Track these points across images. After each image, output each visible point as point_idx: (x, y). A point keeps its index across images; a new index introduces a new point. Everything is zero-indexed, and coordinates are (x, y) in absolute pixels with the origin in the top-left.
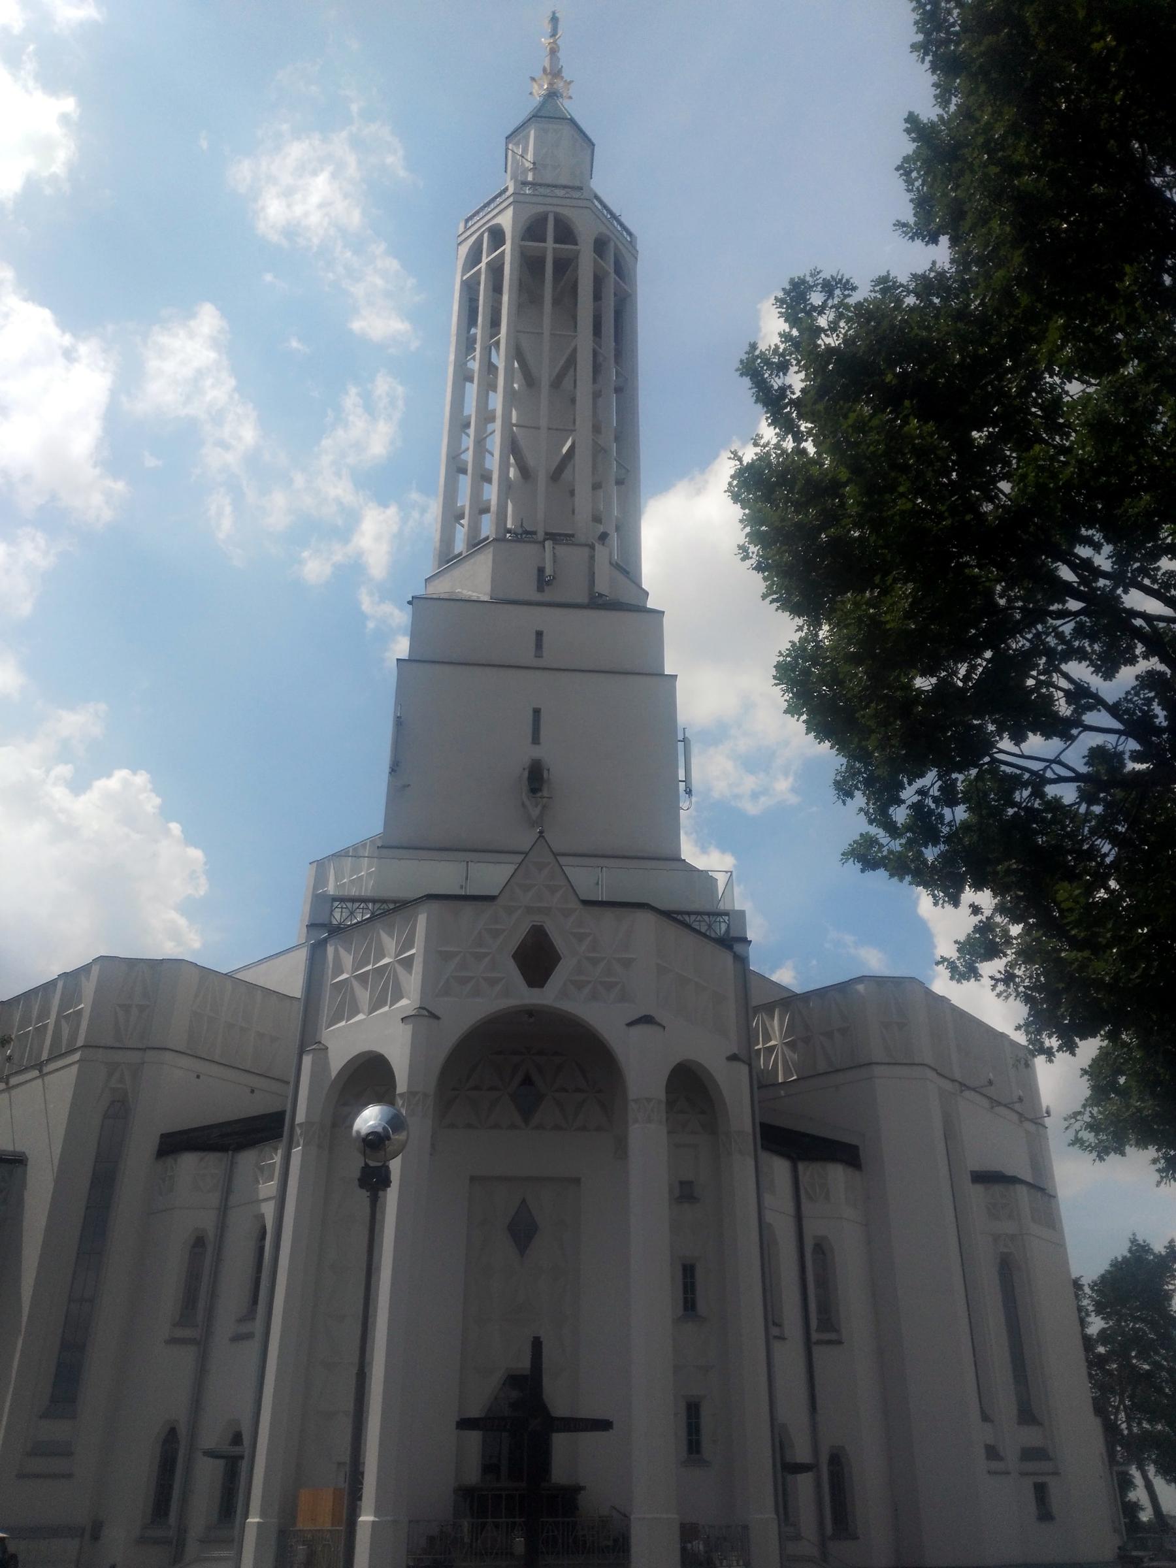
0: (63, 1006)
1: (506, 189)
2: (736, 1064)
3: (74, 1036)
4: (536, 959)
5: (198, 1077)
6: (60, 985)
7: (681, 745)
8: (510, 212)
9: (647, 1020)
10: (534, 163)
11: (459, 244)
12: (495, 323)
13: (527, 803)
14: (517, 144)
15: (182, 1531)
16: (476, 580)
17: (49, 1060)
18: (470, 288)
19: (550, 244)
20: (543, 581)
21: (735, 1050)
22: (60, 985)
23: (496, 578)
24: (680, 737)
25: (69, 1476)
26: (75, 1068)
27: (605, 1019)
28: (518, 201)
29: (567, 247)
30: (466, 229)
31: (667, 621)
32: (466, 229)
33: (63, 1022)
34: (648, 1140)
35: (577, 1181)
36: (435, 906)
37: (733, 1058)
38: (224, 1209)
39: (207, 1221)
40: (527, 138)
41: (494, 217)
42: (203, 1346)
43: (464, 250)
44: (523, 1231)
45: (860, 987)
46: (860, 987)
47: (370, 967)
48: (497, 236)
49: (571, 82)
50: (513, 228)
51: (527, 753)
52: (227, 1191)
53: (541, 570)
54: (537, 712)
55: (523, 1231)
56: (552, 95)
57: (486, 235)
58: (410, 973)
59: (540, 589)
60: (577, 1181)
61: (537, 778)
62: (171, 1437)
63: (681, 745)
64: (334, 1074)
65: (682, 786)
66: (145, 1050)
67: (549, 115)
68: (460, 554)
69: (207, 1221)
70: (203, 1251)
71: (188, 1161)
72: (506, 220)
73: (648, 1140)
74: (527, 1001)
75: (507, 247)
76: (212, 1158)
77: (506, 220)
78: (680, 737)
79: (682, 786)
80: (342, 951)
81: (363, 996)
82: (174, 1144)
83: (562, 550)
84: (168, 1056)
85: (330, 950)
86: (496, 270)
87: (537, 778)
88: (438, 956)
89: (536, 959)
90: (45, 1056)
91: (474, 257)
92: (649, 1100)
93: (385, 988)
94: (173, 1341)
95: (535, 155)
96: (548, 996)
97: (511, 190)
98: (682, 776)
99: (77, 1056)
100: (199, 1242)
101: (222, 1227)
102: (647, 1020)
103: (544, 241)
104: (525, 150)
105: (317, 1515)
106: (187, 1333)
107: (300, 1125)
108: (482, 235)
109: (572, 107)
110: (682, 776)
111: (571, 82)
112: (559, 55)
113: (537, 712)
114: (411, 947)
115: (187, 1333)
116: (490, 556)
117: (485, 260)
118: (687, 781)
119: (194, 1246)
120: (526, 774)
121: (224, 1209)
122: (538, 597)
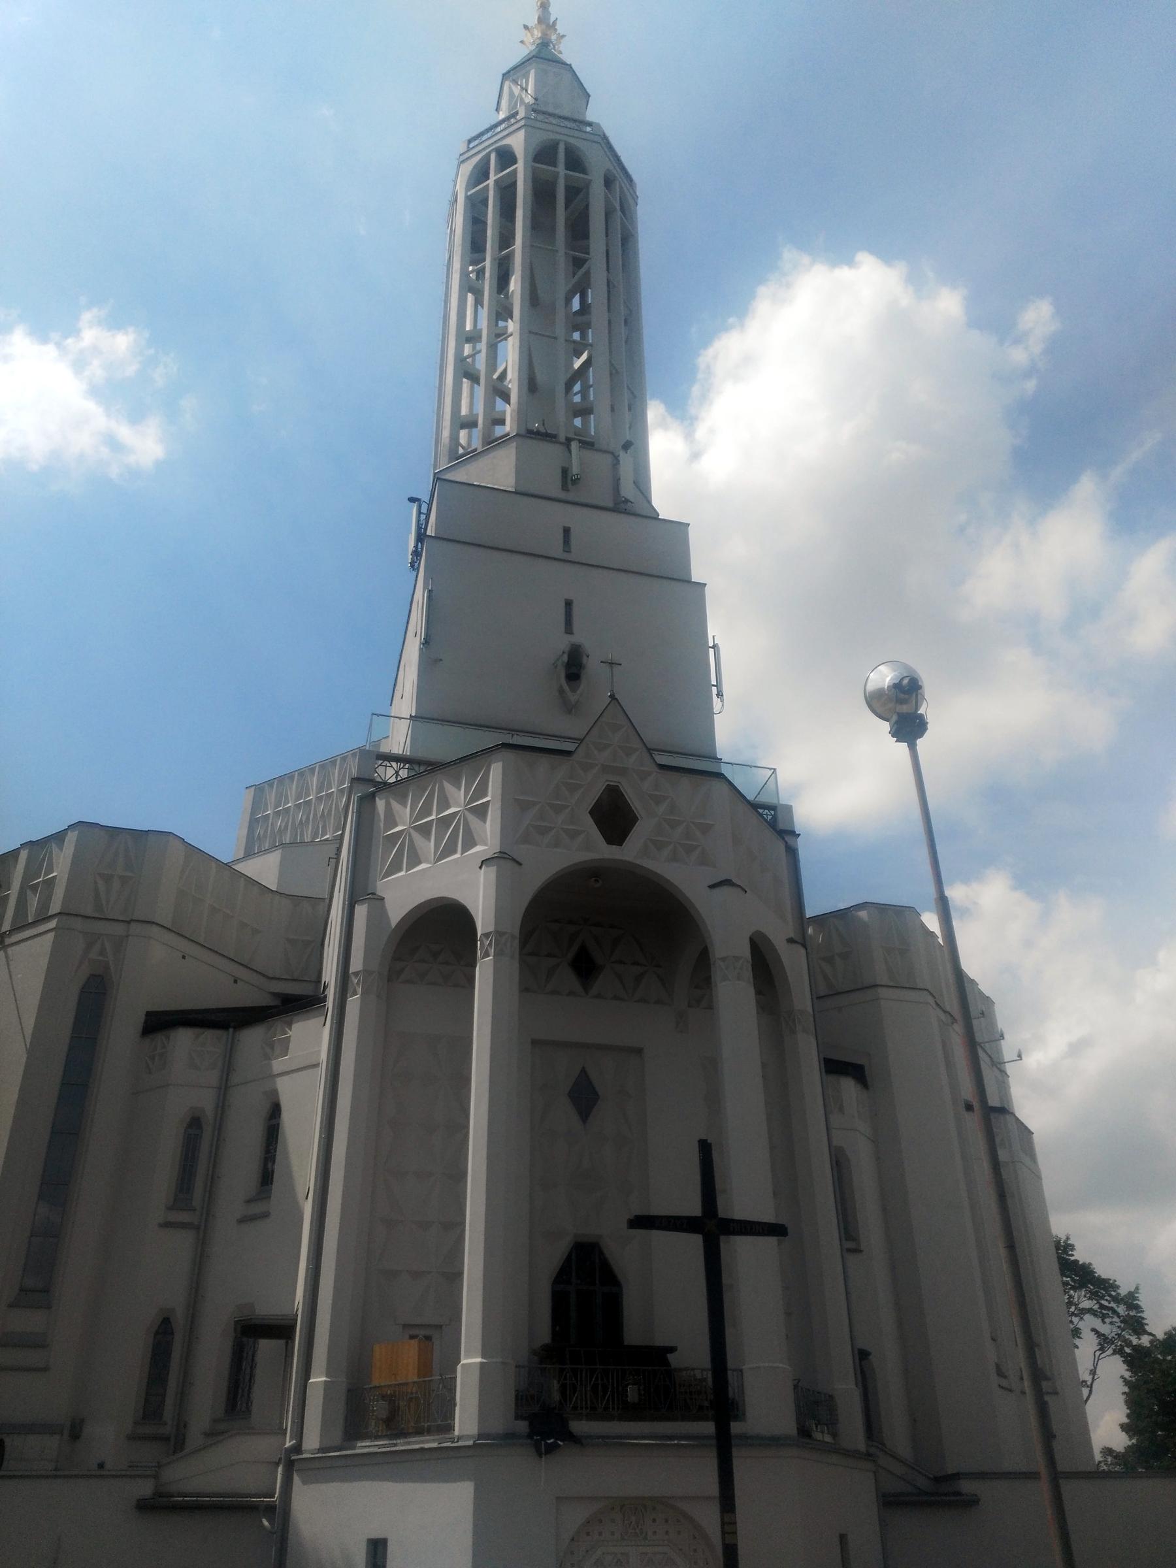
0: (28, 875)
1: (517, 113)
2: (794, 946)
3: (45, 904)
4: (614, 817)
5: (184, 957)
6: (24, 855)
7: (711, 651)
8: (521, 134)
9: (727, 882)
10: (536, 99)
11: (463, 162)
12: (506, 239)
13: (566, 688)
14: (515, 82)
15: (181, 1426)
16: (500, 471)
17: (15, 929)
18: (476, 206)
19: (561, 169)
20: (568, 479)
21: (792, 935)
22: (24, 855)
23: (519, 471)
24: (711, 644)
25: (45, 1369)
26: (51, 936)
27: (687, 879)
28: (528, 126)
29: (577, 174)
30: (469, 150)
31: (693, 535)
32: (469, 150)
33: (29, 892)
34: (734, 995)
35: (639, 1051)
36: (510, 755)
37: (791, 941)
38: (224, 1089)
39: (206, 1101)
40: (528, 73)
41: (508, 135)
42: (202, 1231)
43: (468, 168)
44: (584, 1097)
45: (863, 914)
46: (863, 914)
47: (433, 817)
48: (506, 157)
49: (563, 36)
50: (526, 149)
51: (562, 643)
52: (228, 1069)
53: (565, 472)
54: (569, 604)
55: (584, 1097)
56: (544, 44)
57: (493, 156)
58: (485, 821)
59: (565, 487)
60: (639, 1051)
61: (573, 667)
62: (164, 1328)
63: (711, 651)
64: (394, 922)
65: (714, 689)
66: (129, 922)
67: (544, 56)
68: (475, 450)
69: (206, 1101)
70: (198, 1139)
71: (183, 1039)
72: (517, 142)
73: (734, 995)
74: (607, 856)
75: (520, 166)
76: (209, 1035)
77: (517, 142)
78: (711, 644)
79: (714, 689)
80: (395, 805)
81: (428, 846)
82: (159, 1023)
83: (587, 454)
84: (155, 930)
85: (380, 804)
86: (507, 191)
87: (573, 667)
88: (516, 805)
89: (614, 817)
90: (6, 927)
91: (481, 173)
92: (737, 958)
93: (455, 837)
94: (167, 1225)
95: (536, 89)
96: (630, 852)
97: (521, 114)
98: (714, 682)
99: (52, 924)
100: (195, 1123)
101: (222, 1106)
102: (727, 882)
103: (554, 164)
104: (527, 84)
105: (398, 1364)
106: (184, 1217)
107: (356, 974)
108: (488, 156)
109: (567, 52)
110: (714, 682)
111: (563, 36)
112: (551, 9)
113: (569, 604)
114: (486, 795)
115: (184, 1217)
116: (514, 451)
117: (493, 178)
118: (718, 685)
119: (190, 1126)
120: (565, 658)
121: (224, 1089)
122: (562, 495)
